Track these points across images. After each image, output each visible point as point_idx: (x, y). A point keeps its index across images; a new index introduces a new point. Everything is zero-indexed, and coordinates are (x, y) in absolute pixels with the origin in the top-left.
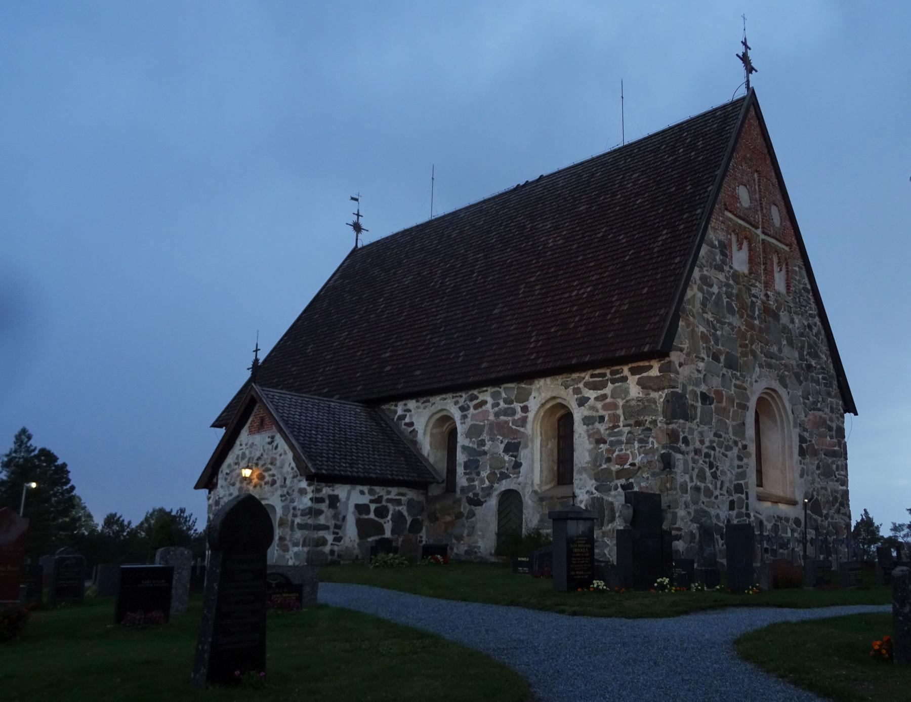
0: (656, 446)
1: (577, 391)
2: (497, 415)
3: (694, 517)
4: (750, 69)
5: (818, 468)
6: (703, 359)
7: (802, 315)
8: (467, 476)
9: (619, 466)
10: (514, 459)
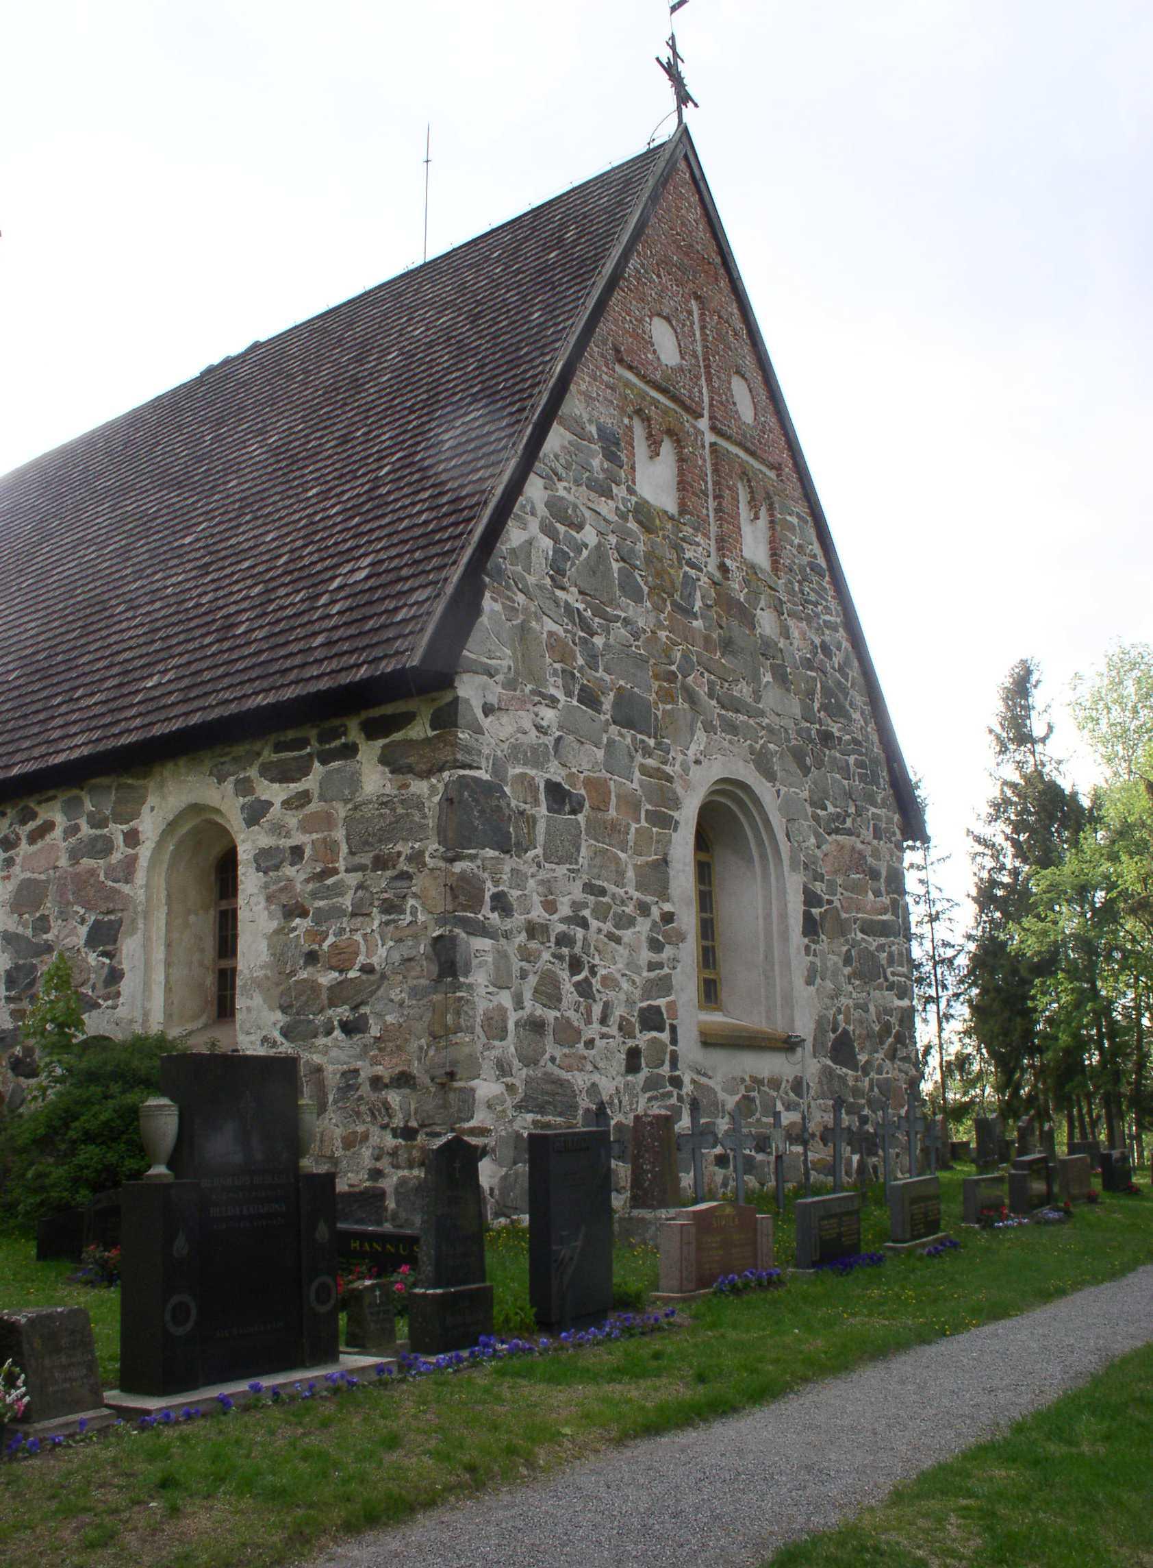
0: (421, 918)
1: (244, 787)
2: (75, 856)
3: (526, 1098)
4: (683, 97)
5: (847, 961)
6: (553, 702)
7: (809, 623)
8: (12, 1006)
9: (337, 974)
10: (108, 961)
